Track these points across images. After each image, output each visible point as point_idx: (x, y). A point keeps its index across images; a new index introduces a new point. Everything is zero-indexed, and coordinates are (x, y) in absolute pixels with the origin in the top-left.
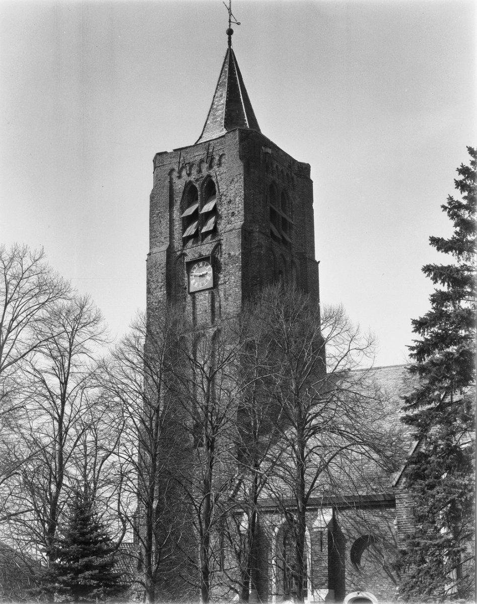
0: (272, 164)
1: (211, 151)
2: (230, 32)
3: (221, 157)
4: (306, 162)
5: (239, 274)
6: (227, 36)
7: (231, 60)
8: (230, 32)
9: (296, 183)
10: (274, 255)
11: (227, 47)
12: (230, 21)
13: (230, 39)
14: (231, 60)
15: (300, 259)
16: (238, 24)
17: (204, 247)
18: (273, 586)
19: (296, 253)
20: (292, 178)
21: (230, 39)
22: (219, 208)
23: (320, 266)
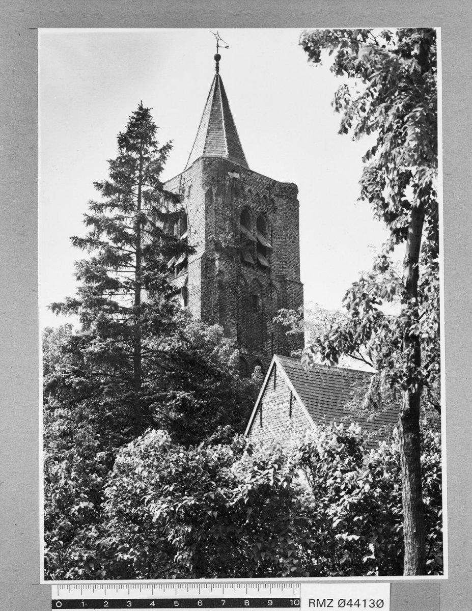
0: (243, 188)
1: (182, 183)
2: (218, 58)
3: (190, 187)
4: (289, 181)
5: (199, 303)
6: (215, 62)
7: (218, 88)
8: (218, 58)
9: (277, 204)
10: (245, 280)
11: (215, 73)
12: (218, 46)
13: (217, 64)
14: (218, 88)
15: (280, 282)
16: (227, 47)
17: (178, 280)
18: (406, 567)
19: (277, 276)
20: (272, 200)
21: (217, 64)
22: (270, 217)
23: (304, 287)
